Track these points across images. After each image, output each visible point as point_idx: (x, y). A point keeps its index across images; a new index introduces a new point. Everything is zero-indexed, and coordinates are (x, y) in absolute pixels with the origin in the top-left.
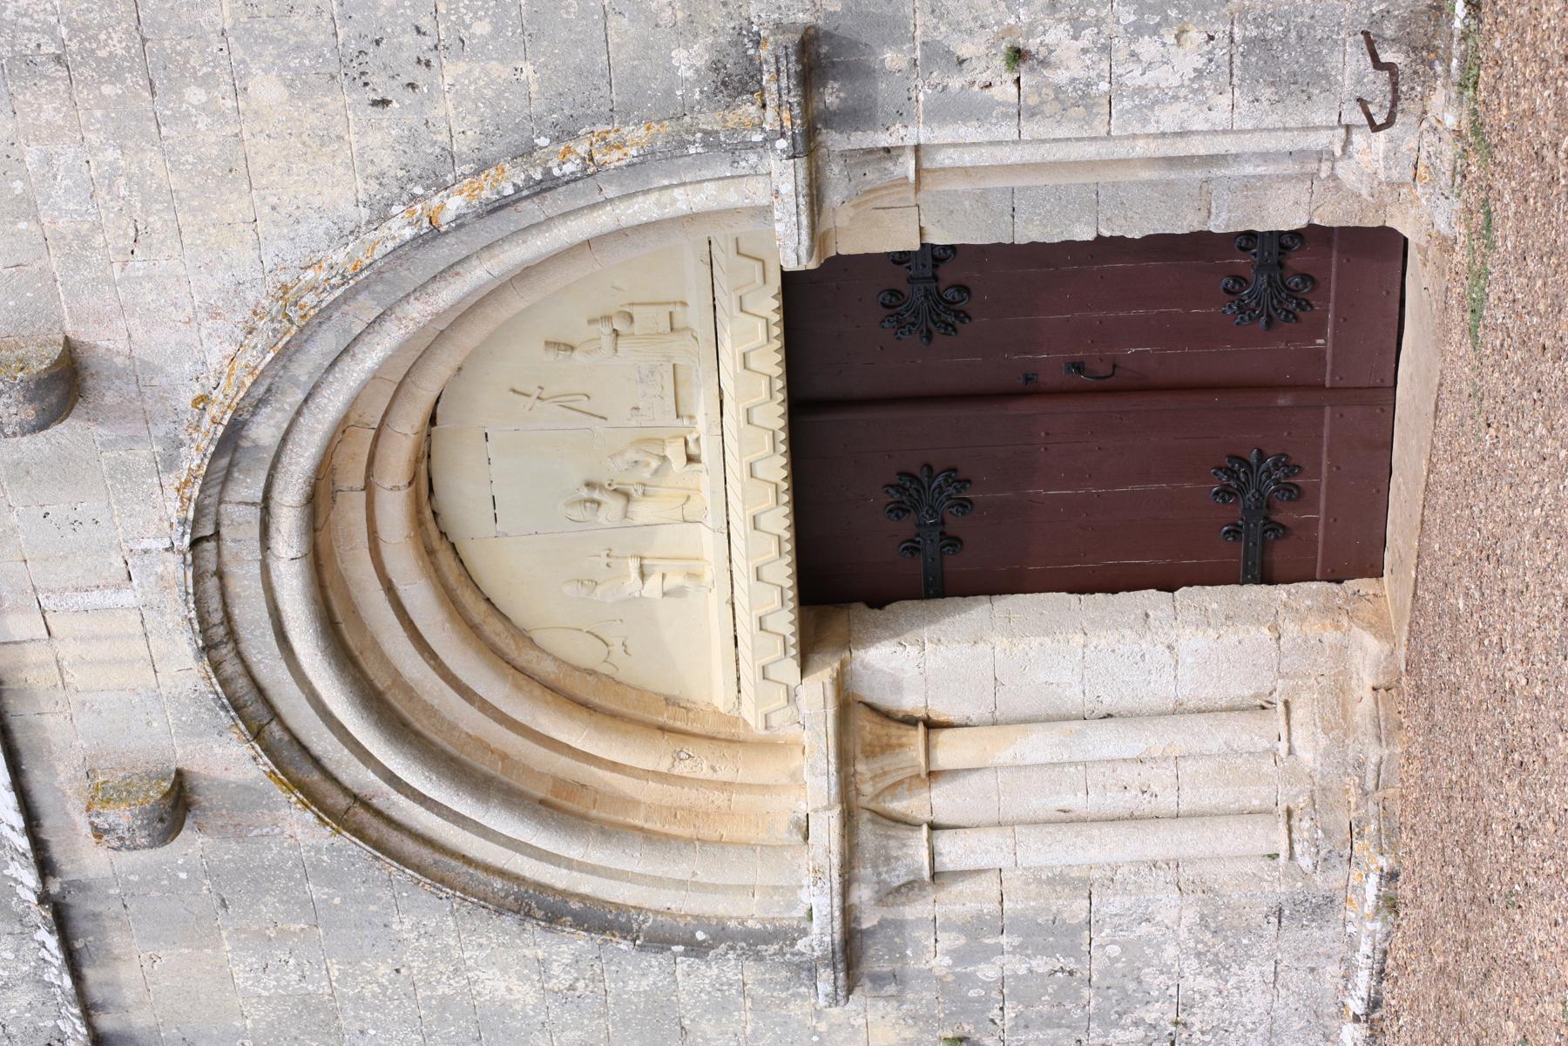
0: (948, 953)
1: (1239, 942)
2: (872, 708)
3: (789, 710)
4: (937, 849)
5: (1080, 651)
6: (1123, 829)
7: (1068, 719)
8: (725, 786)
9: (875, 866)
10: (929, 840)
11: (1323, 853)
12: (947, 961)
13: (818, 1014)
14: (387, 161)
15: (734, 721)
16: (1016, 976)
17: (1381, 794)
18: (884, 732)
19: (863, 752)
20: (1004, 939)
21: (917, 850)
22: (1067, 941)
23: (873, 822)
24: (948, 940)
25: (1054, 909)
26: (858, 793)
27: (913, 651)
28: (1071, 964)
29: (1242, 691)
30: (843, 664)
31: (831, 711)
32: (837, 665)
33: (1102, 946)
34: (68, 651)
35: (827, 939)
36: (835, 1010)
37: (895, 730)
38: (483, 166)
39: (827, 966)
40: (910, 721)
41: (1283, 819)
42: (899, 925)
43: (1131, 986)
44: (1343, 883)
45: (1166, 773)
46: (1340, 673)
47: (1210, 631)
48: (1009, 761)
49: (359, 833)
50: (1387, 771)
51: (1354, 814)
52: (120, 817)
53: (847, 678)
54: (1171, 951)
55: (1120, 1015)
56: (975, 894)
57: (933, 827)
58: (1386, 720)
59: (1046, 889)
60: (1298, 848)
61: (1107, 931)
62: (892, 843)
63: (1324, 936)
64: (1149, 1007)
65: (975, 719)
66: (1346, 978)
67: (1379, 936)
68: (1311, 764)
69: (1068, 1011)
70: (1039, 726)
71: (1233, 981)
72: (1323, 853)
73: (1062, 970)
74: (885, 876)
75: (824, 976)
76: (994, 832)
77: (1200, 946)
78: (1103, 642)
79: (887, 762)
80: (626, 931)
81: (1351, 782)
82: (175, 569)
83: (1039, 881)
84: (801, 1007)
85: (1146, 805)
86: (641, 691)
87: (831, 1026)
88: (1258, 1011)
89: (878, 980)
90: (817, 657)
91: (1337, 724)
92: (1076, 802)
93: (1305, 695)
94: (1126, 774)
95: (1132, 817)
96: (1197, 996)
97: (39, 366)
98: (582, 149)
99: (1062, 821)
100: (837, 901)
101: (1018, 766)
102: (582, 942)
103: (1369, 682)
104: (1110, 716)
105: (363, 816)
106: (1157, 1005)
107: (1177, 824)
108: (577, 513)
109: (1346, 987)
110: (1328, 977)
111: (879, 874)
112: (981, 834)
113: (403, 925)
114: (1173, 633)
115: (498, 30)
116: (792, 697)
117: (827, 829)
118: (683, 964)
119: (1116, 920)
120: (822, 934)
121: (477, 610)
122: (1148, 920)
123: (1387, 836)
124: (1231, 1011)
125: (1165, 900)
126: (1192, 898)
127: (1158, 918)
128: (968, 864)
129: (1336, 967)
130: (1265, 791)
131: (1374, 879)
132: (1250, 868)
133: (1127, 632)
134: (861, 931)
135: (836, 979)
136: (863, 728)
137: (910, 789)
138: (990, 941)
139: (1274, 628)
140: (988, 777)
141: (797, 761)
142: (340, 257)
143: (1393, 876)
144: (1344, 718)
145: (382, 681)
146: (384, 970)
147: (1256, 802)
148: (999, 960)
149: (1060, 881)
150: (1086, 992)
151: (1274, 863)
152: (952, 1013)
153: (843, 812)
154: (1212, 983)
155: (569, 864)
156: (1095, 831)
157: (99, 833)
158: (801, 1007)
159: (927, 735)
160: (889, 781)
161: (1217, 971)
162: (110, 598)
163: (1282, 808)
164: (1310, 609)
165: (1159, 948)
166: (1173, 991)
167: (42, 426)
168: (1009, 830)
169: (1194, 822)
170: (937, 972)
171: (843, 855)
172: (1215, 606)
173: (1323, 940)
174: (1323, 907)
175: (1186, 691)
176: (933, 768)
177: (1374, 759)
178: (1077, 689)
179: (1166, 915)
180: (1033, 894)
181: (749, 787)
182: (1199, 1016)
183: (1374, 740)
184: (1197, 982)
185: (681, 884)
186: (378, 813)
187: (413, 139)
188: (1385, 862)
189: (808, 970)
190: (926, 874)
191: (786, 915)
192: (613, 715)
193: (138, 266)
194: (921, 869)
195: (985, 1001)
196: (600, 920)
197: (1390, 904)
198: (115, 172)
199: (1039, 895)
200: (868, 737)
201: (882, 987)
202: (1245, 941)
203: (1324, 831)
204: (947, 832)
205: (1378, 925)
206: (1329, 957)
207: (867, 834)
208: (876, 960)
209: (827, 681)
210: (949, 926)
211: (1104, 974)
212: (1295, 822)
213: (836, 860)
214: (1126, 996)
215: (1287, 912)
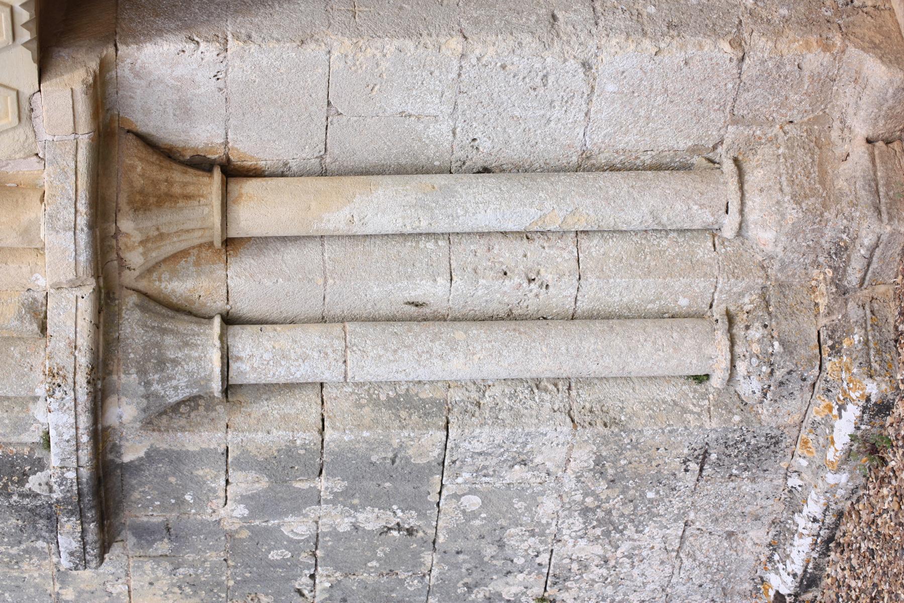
0: (244, 499)
1: (643, 495)
2: (147, 142)
3: (22, 133)
4: (234, 352)
5: (455, 64)
6: (500, 331)
7: (427, 172)
9: (142, 372)
10: (223, 337)
11: (779, 374)
12: (241, 511)
13: (62, 577)
16: (335, 534)
17: (866, 292)
18: (163, 176)
19: (130, 202)
20: (322, 484)
21: (201, 357)
22: (409, 488)
23: (142, 308)
24: (244, 482)
25: (395, 442)
26: (123, 265)
27: (209, 50)
28: (411, 519)
29: (674, 140)
30: (104, 66)
31: (84, 140)
32: (94, 65)
33: (457, 497)
35: (71, 475)
36: (87, 574)
37: (179, 176)
39: (71, 513)
40: (201, 164)
41: (723, 325)
42: (176, 459)
43: (489, 551)
44: (797, 418)
45: (561, 255)
46: (816, 120)
47: (646, 43)
48: (343, 229)
50: (882, 259)
51: (823, 321)
53: (111, 90)
54: (549, 505)
55: (470, 588)
56: (285, 418)
57: (229, 320)
58: (887, 185)
59: (386, 415)
60: (742, 367)
61: (466, 475)
62: (169, 340)
63: (758, 490)
64: (510, 579)
65: (294, 165)
66: (773, 546)
67: (841, 493)
68: (769, 248)
69: (401, 582)
70: (387, 179)
71: (625, 547)
72: (779, 374)
73: (399, 527)
74: (156, 387)
75: (68, 527)
76: (315, 330)
77: (589, 500)
78: (491, 51)
79: (166, 219)
81: (822, 276)
83: (376, 403)
84: (39, 567)
85: (532, 299)
87: (80, 593)
88: (651, 586)
89: (146, 534)
90: (64, 53)
91: (812, 185)
92: (434, 291)
93: (765, 151)
94: (508, 253)
95: (510, 317)
96: (575, 566)
99: (412, 319)
100: (84, 421)
101: (354, 236)
103: (862, 130)
104: (486, 170)
106: (520, 577)
107: (575, 327)
109: (770, 559)
110: (749, 544)
111: (148, 384)
112: (297, 331)
114: (592, 43)
116: (25, 112)
117: (73, 317)
119: (480, 461)
120: (63, 467)
122: (524, 463)
123: (878, 352)
124: (616, 586)
125: (551, 435)
126: (589, 432)
127: (538, 460)
128: (279, 374)
129: (762, 533)
130: (701, 285)
131: (852, 412)
132: (669, 393)
133: (527, 39)
134: (124, 467)
135: (83, 531)
136: (133, 167)
137: (197, 264)
138: (304, 485)
139: (737, 43)
140: (312, 252)
141: (34, 212)
143: (884, 408)
144: (822, 182)
147: (683, 302)
148: (313, 511)
149: (405, 403)
150: (428, 558)
151: (701, 388)
152: (245, 581)
153: (98, 291)
154: (598, 550)
156: (459, 333)
158: (39, 567)
160: (168, 249)
161: (607, 534)
163: (718, 312)
164: (786, 20)
165: (534, 501)
166: (544, 558)
168: (337, 328)
169: (598, 325)
170: (227, 526)
171: (95, 353)
172: (652, 10)
173: (754, 496)
174: (760, 451)
175: (598, 138)
176: (232, 234)
177: (868, 240)
178: (445, 127)
179: (549, 457)
180: (367, 421)
182: (574, 592)
183: (870, 213)
184: (577, 546)
188: (873, 389)
189: (43, 517)
190: (216, 386)
191: (14, 439)
194: (208, 379)
195: (291, 566)
197: (872, 449)
199: (375, 421)
200: (139, 183)
201: (151, 543)
202: (650, 495)
203: (782, 343)
204: (249, 328)
205: (843, 478)
206: (757, 518)
207: (133, 326)
208: (143, 507)
209: (79, 88)
210: (246, 462)
211: (454, 534)
212: (739, 330)
213: (84, 360)
214: (480, 563)
215: (714, 457)
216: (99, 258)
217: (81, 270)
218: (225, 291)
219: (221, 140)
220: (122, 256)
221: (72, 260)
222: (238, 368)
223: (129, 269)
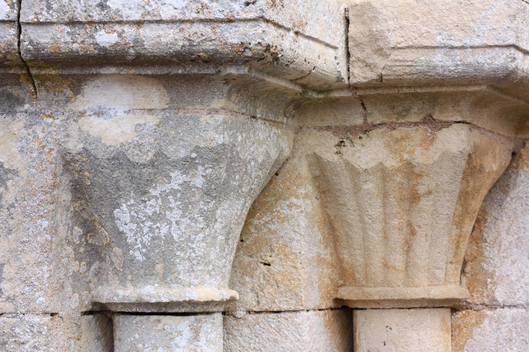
176: (118, 320)
190: (117, 292)
216: (386, 91)
217: (409, 55)
218: (285, 307)
219: (500, 295)
220: (374, 133)
221: (439, 40)
222: (180, 333)
223: (341, 143)
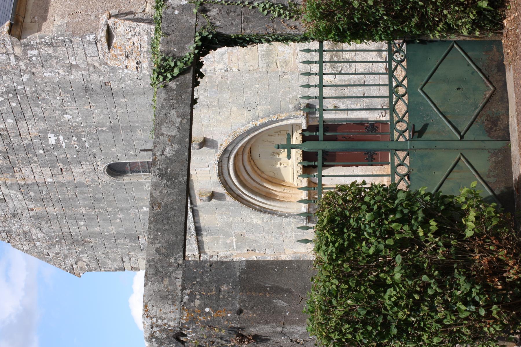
2: (313, 182)
8: (291, 194)
14: (250, 117)
15: (293, 184)
34: (198, 175)
38: (263, 118)
49: (238, 200)
52: (204, 198)
80: (276, 214)
82: (216, 166)
86: (279, 179)
97: (200, 141)
98: (276, 117)
102: (269, 215)
105: (239, 198)
108: (271, 156)
113: (243, 212)
115: (266, 103)
116: (301, 181)
118: (284, 219)
121: (256, 169)
142: (242, 128)
145: (242, 179)
146: (239, 219)
155: (268, 205)
157: (201, 200)
159: (302, 214)
162: (206, 169)
167: (200, 148)
181: (293, 194)
185: (284, 208)
186: (241, 197)
187: (254, 115)
192: (275, 183)
193: (215, 128)
196: (272, 213)
198: (213, 118)
